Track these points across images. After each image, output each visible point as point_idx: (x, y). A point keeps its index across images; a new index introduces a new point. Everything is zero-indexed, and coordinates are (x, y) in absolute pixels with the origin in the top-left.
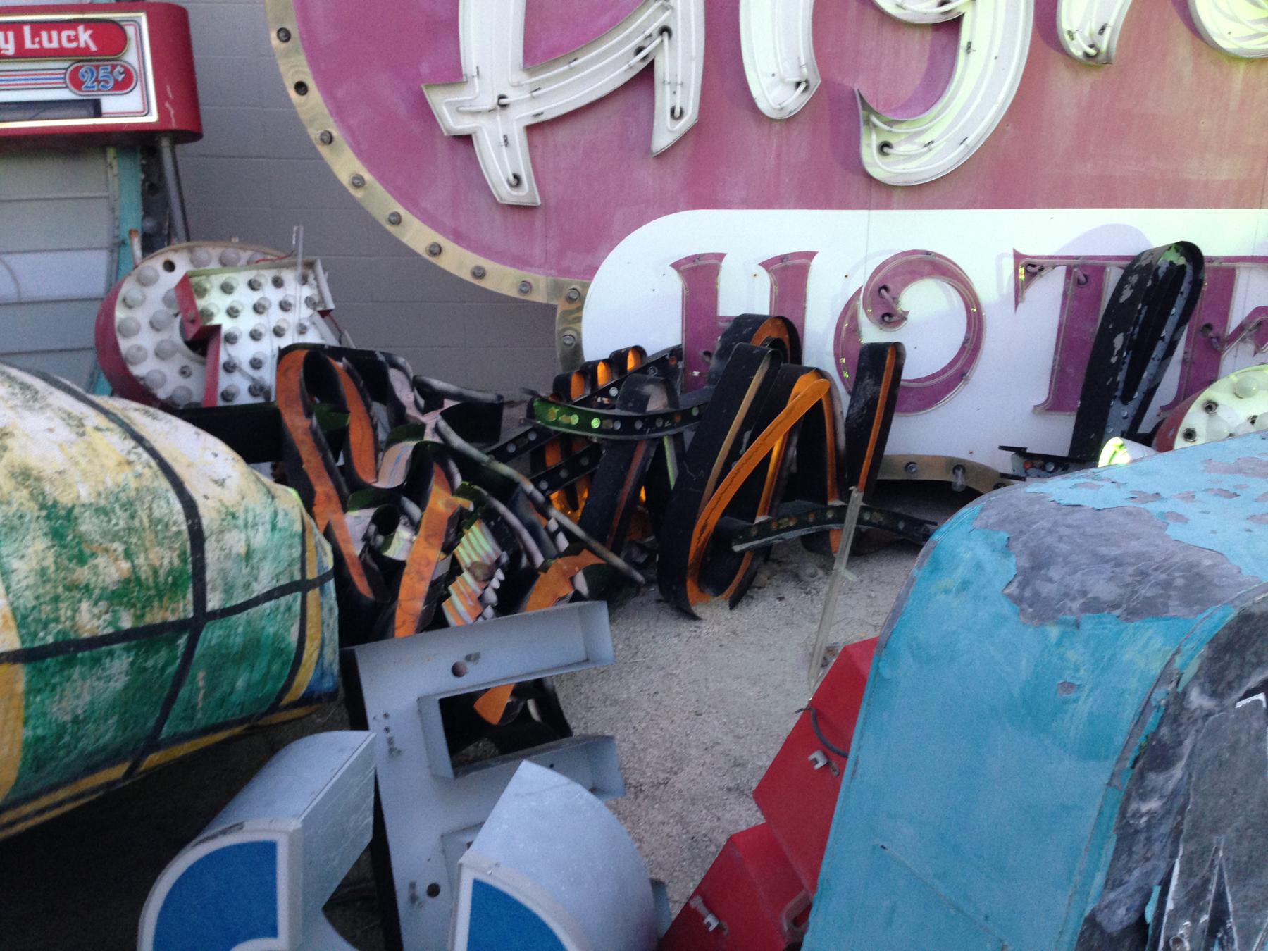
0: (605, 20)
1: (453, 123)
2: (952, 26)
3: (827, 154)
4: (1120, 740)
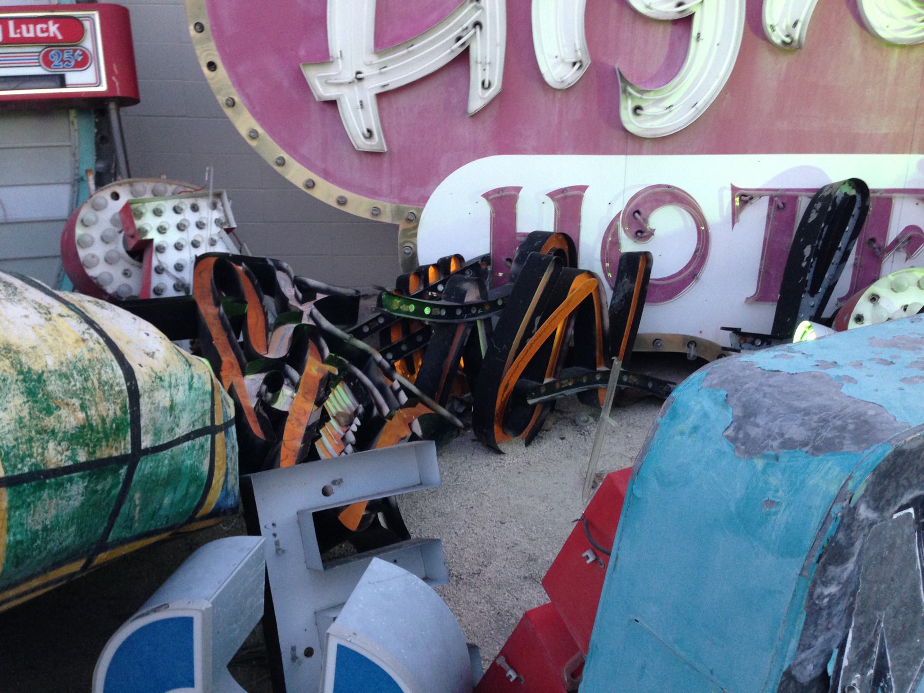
0: (434, 16)
1: (323, 92)
2: (686, 21)
3: (596, 114)
4: (808, 543)
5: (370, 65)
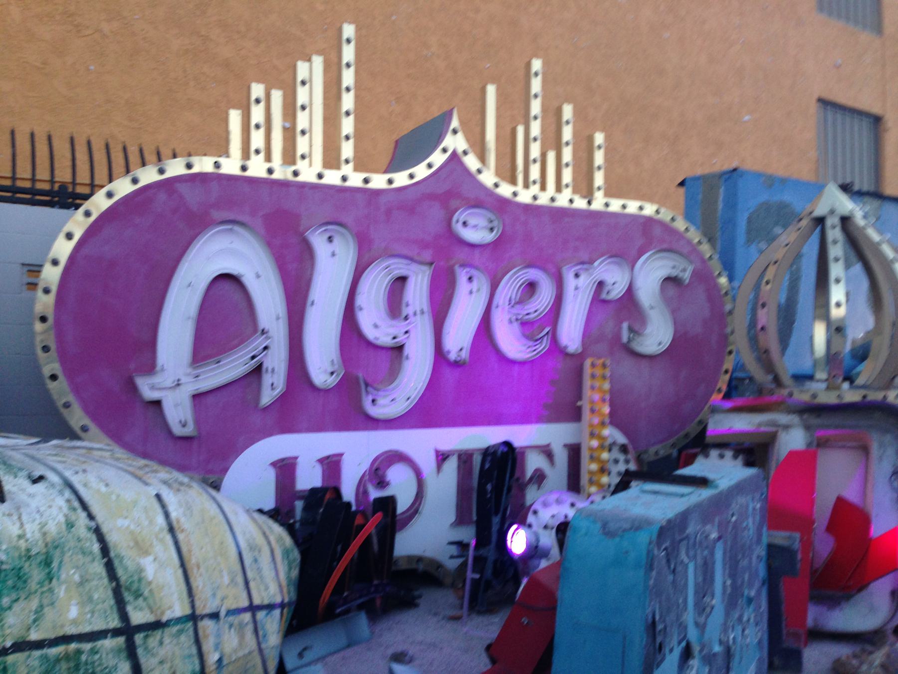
0: (236, 342)
1: (149, 394)
2: (400, 348)
3: (346, 407)
4: (644, 562)
5: (189, 375)
